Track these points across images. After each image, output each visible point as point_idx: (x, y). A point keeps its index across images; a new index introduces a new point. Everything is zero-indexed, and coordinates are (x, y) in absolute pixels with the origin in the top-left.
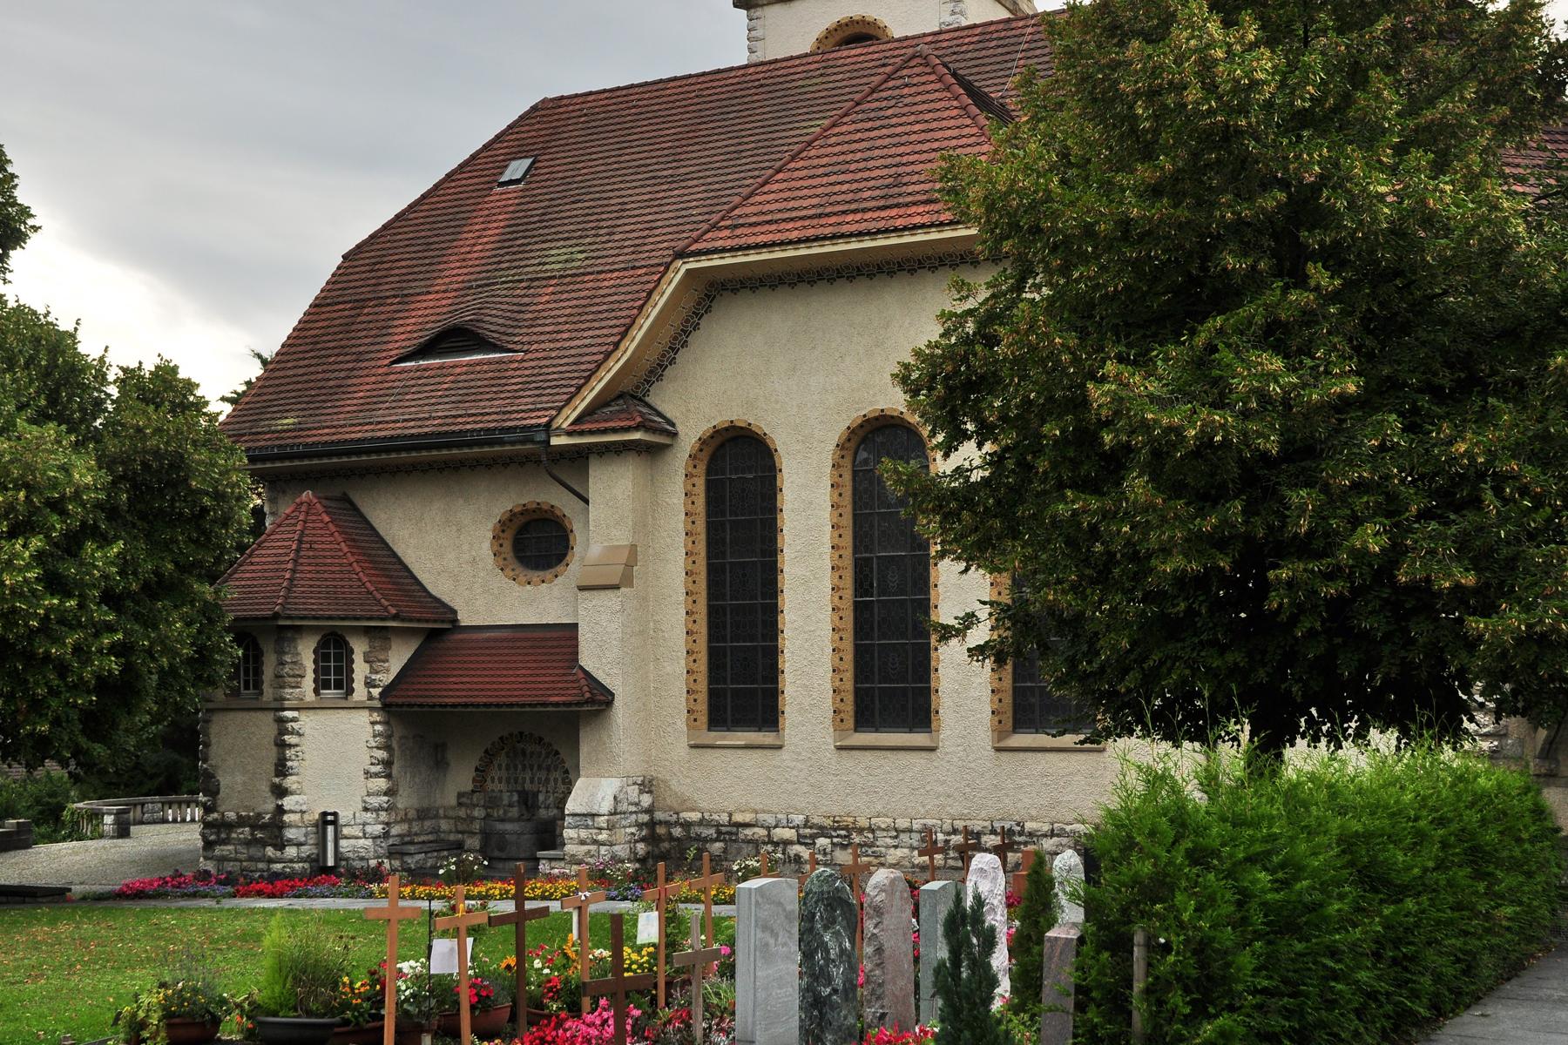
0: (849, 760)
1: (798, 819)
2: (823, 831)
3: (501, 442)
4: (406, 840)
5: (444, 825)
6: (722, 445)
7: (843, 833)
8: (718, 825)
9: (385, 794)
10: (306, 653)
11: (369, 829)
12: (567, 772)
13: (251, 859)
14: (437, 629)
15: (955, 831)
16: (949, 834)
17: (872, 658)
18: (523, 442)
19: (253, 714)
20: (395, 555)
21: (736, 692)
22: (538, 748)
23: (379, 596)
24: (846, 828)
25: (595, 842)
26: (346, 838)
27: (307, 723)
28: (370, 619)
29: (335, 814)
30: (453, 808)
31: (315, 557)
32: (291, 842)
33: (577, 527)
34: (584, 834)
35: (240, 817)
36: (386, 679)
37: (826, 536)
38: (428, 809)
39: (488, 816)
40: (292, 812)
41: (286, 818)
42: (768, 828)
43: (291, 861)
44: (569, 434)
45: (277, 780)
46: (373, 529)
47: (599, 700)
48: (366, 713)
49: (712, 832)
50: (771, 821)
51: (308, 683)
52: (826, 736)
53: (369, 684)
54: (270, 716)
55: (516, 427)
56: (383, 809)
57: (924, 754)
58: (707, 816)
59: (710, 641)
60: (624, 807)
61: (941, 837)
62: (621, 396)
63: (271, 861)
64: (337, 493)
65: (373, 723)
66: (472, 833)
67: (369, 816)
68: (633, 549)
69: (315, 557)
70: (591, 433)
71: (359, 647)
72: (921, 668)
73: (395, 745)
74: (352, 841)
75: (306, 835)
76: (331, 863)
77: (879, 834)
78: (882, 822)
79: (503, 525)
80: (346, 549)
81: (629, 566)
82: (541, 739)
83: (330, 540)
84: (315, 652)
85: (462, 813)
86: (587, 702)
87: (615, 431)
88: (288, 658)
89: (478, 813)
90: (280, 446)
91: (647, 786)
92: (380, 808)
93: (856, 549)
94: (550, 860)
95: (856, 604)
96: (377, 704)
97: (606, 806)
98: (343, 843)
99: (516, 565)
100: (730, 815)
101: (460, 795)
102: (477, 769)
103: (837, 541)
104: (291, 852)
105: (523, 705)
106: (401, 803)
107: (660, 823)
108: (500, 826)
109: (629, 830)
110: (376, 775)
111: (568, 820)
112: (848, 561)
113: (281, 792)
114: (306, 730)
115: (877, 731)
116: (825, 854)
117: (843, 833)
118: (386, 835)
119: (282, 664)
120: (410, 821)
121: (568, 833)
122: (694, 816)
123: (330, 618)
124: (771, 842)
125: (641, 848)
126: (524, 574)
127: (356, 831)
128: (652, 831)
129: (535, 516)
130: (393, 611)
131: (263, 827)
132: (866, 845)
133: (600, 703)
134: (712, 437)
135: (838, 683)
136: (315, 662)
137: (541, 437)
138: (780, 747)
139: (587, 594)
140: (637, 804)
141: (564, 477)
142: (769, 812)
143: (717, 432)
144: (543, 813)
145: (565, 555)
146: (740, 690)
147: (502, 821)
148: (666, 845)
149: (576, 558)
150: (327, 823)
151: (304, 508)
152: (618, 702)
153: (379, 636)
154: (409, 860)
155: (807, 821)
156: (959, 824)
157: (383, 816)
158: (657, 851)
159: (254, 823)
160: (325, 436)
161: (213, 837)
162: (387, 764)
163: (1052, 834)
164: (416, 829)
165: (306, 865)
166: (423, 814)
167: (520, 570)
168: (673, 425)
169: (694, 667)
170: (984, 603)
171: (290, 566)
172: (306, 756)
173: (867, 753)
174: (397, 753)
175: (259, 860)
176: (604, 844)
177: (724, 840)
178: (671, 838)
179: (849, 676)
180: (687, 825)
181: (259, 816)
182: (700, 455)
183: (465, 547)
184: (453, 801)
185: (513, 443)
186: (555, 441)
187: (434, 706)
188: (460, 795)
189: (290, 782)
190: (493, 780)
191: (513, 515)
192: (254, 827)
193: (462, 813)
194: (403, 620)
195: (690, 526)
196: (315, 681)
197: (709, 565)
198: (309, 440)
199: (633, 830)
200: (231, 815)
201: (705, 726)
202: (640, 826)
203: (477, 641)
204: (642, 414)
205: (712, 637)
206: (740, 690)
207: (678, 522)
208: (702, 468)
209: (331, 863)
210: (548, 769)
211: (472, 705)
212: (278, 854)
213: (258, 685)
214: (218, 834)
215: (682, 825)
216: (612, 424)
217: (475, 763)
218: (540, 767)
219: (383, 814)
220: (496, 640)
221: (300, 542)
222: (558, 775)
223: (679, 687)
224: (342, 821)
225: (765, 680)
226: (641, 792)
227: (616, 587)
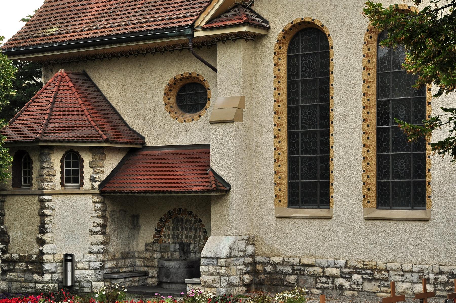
0: (374, 226)
1: (341, 263)
2: (356, 270)
3: (167, 37)
4: (114, 270)
5: (138, 262)
6: (297, 35)
7: (369, 272)
8: (293, 265)
9: (102, 244)
10: (56, 161)
11: (92, 264)
12: (205, 232)
13: (26, 281)
14: (133, 148)
15: (441, 273)
16: (437, 274)
17: (388, 163)
18: (179, 36)
19: (27, 197)
20: (111, 106)
21: (304, 184)
22: (190, 218)
23: (98, 129)
24: (371, 269)
25: (218, 274)
26: (79, 269)
27: (55, 202)
28: (92, 142)
29: (72, 255)
30: (142, 252)
31: (63, 107)
32: (47, 272)
33: (211, 87)
34: (212, 269)
35: (20, 256)
36: (103, 177)
37: (360, 87)
38: (128, 253)
39: (162, 257)
40: (48, 254)
41: (45, 257)
42: (323, 268)
43: (47, 282)
44: (205, 29)
45: (40, 235)
46: (99, 91)
47: (221, 189)
48: (91, 196)
49: (289, 269)
50: (325, 263)
51: (57, 179)
52: (358, 211)
53: (93, 180)
54: (36, 198)
55: (175, 27)
56: (100, 253)
57: (421, 223)
58: (286, 259)
59: (289, 154)
60: (236, 253)
61: (432, 276)
62: (236, 6)
63: (36, 282)
64: (80, 71)
65: (95, 203)
66: (153, 267)
67: (92, 257)
68: (243, 98)
69: (63, 107)
70: (217, 28)
71: (87, 159)
72: (420, 168)
73: (108, 215)
74: (83, 271)
75: (56, 267)
76: (69, 283)
77: (392, 273)
78: (394, 266)
79: (171, 87)
80: (81, 102)
81: (240, 108)
82: (191, 212)
83: (73, 97)
84: (62, 161)
85: (148, 255)
86: (213, 190)
87: (231, 26)
88: (45, 165)
89: (156, 255)
90: (47, 43)
91: (250, 241)
92: (99, 252)
93: (378, 96)
94: (193, 284)
95: (378, 129)
96: (97, 191)
97: (225, 253)
98: (77, 272)
99: (178, 110)
100: (300, 259)
101: (147, 245)
102: (156, 230)
103: (366, 90)
104: (47, 277)
105: (177, 192)
106: (112, 249)
107: (259, 263)
108: (167, 263)
109: (239, 267)
110: (97, 233)
111: (203, 261)
112: (373, 103)
113: (42, 242)
114: (56, 207)
115: (391, 209)
116: (358, 284)
117: (369, 272)
118: (102, 268)
119: (42, 168)
120: (117, 260)
121: (203, 269)
122: (279, 259)
123: (69, 141)
124: (324, 276)
125: (247, 278)
126: (182, 115)
127: (85, 265)
128: (254, 268)
129: (188, 81)
130: (105, 137)
131: (33, 262)
132: (383, 280)
133: (222, 191)
134: (290, 29)
135: (366, 179)
136: (62, 167)
137: (188, 32)
138: (330, 218)
139: (215, 126)
140: (244, 252)
141: (203, 57)
142: (324, 258)
143: (294, 26)
144: (193, 256)
145: (205, 104)
146: (308, 183)
147: (169, 260)
148: (262, 276)
149: (211, 105)
150: (67, 261)
151: (58, 79)
152: (232, 191)
153: (99, 152)
154: (114, 282)
155: (347, 264)
156: (445, 269)
157: (101, 257)
158: (257, 280)
159: (27, 260)
160: (71, 37)
161: (6, 268)
162: (103, 226)
164: (121, 263)
165: (56, 285)
166: (125, 256)
167: (180, 113)
168: (267, 22)
169: (279, 169)
170: (446, 110)
171: (48, 112)
172: (56, 222)
173: (385, 223)
174: (109, 220)
175: (30, 281)
176: (223, 276)
177: (296, 274)
178: (265, 272)
179: (373, 174)
180: (274, 265)
181: (30, 256)
182: (283, 41)
183: (149, 100)
184: (142, 248)
185: (173, 37)
186: (196, 34)
187: (128, 193)
188: (147, 245)
189: (46, 237)
191: (176, 81)
192: (27, 263)
193: (148, 255)
194: (111, 143)
195: (277, 84)
196: (62, 178)
197: (289, 108)
198: (62, 40)
199: (242, 267)
200: (16, 256)
201: (286, 205)
202: (246, 265)
203: (155, 155)
204: (247, 16)
205: (290, 151)
206: (308, 183)
207: (271, 82)
208: (285, 49)
209: (69, 283)
210: (196, 231)
211: (149, 192)
212: (40, 278)
213: (30, 180)
214: (9, 266)
215: (271, 264)
216: (230, 23)
217: (155, 226)
218: (191, 229)
219: (100, 255)
220: (165, 154)
221: (55, 98)
222: (201, 233)
223: (271, 180)
224: (76, 259)
225: (322, 177)
226: (247, 244)
227: (232, 121)
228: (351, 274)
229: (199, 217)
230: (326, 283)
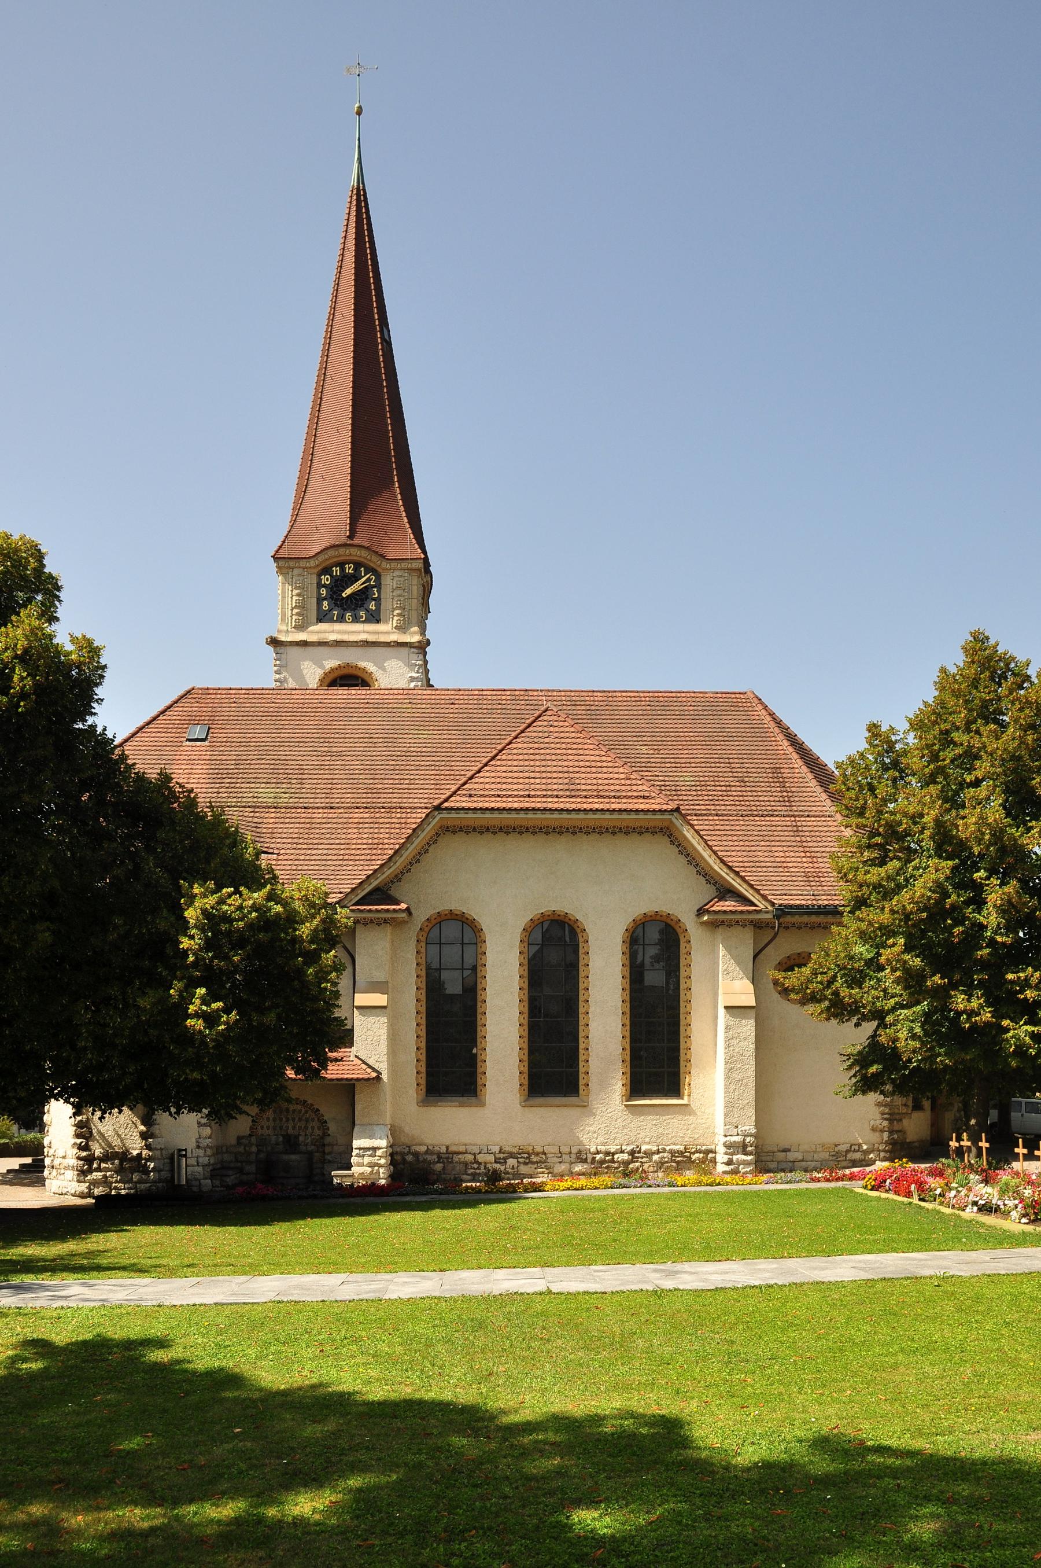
2: (512, 1155)
15: (598, 1153)
58: (431, 1148)
65: (883, 1114)
67: (201, 1152)
110: (205, 1125)
121: (354, 1160)
163: (658, 1152)
177: (443, 1162)
188: (239, 1138)
190: (262, 1128)
218: (300, 1120)
228: (505, 1159)
229: (316, 1107)
230: (478, 1168)
